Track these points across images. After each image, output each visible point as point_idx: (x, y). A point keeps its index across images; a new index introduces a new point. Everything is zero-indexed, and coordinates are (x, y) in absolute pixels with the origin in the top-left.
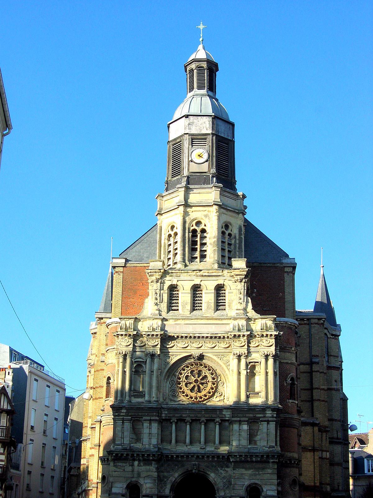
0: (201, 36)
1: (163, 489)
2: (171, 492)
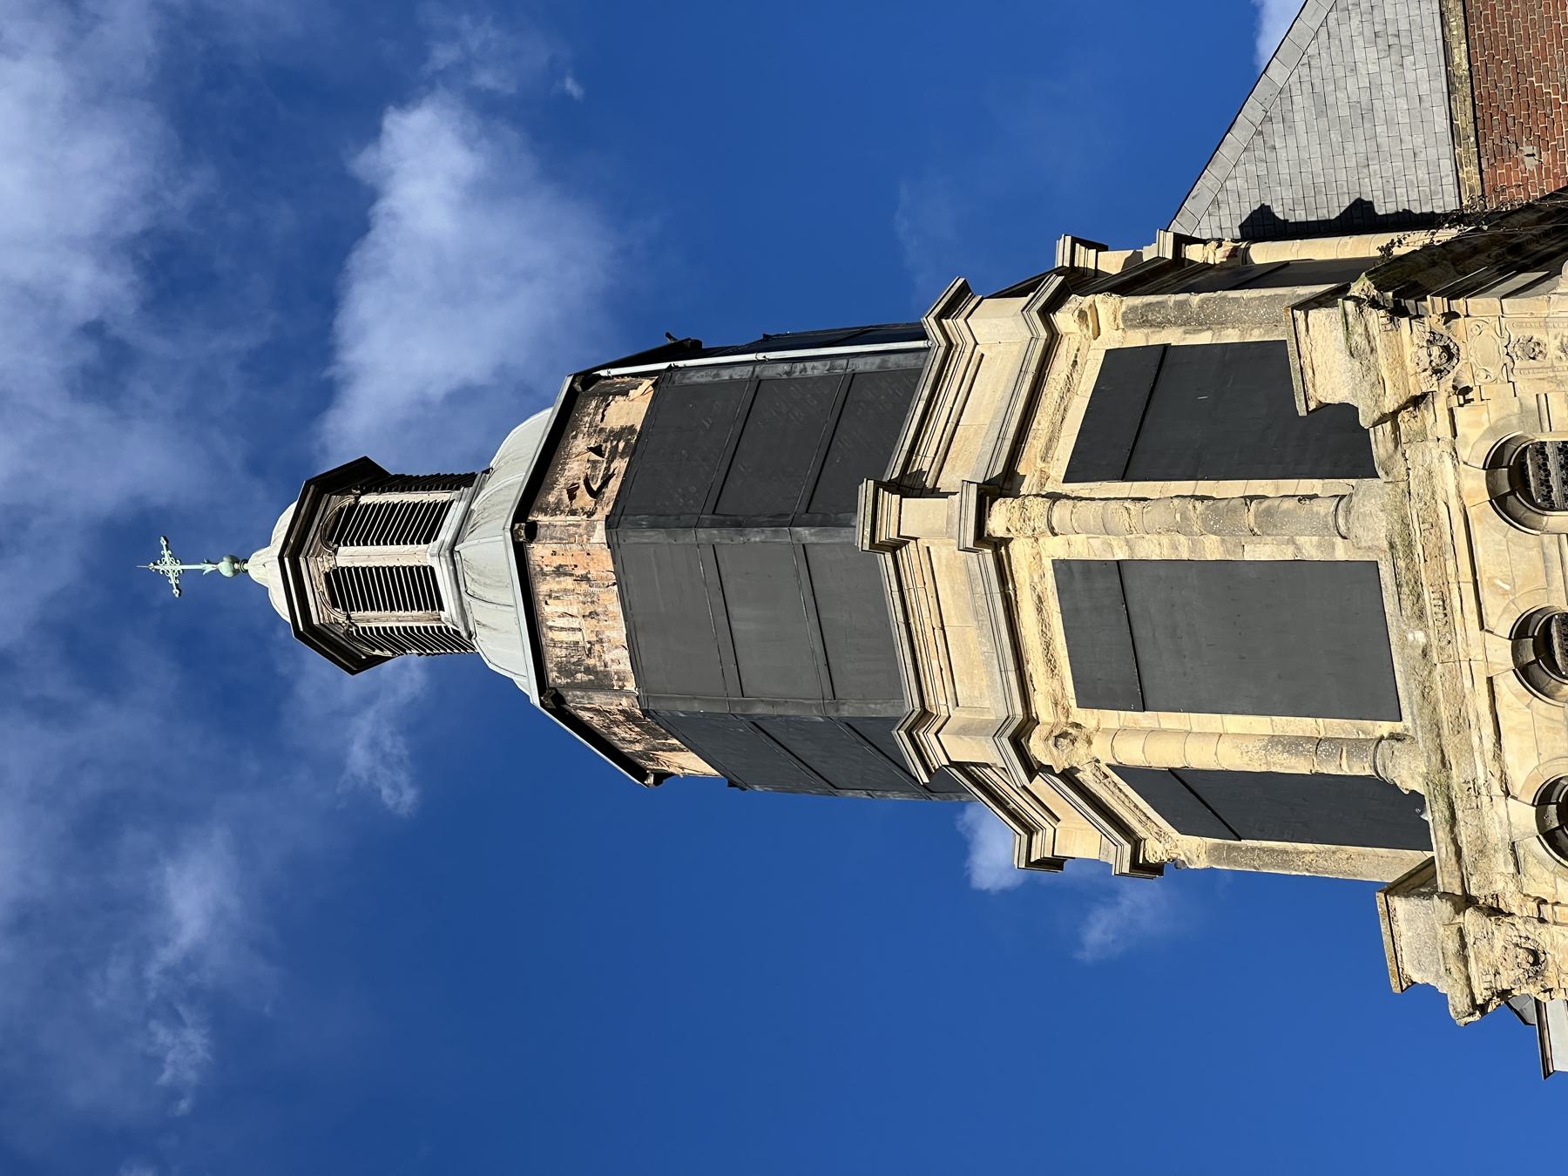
0: (209, 568)
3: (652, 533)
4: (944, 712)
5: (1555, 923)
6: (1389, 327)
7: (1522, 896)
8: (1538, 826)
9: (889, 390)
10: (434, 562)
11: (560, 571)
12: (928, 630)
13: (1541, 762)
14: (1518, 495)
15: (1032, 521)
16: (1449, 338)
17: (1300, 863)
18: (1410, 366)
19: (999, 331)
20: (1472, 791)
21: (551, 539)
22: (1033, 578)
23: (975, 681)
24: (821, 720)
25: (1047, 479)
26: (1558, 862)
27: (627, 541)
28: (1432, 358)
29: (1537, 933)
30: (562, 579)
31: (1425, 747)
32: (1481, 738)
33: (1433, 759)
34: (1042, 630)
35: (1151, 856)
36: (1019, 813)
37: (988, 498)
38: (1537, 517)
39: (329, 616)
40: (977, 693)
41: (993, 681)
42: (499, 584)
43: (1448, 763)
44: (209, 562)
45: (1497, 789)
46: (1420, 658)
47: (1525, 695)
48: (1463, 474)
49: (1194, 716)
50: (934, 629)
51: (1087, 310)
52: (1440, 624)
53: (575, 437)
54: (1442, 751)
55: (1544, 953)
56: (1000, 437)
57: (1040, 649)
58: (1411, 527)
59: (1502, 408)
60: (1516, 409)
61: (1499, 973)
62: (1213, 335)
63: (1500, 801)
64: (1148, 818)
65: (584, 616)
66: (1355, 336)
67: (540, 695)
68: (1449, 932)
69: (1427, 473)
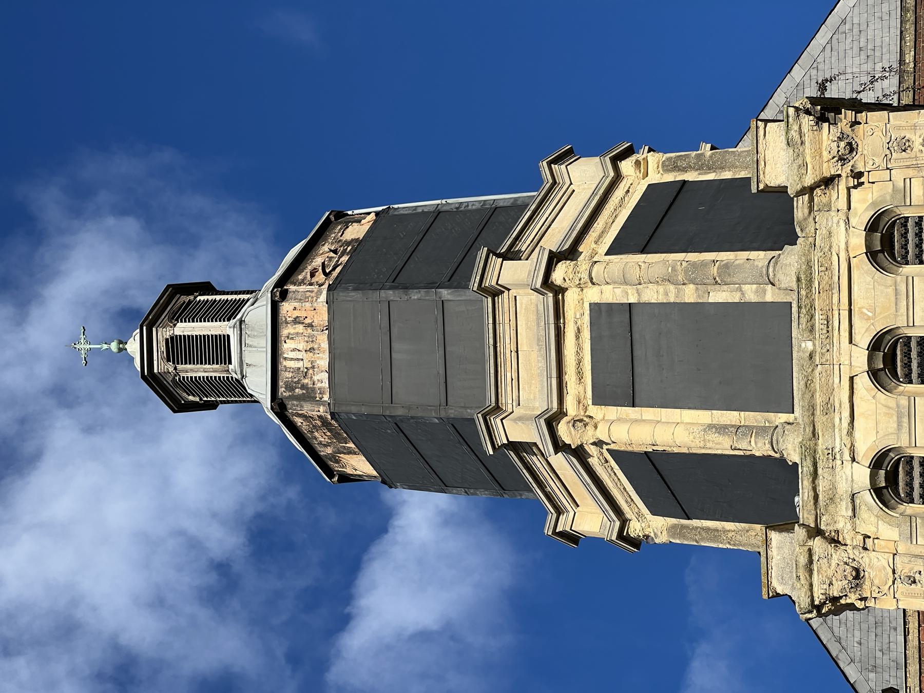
3: (353, 294)
4: (510, 409)
5: (874, 551)
6: (815, 128)
7: (855, 532)
8: (870, 482)
9: (515, 216)
10: (230, 332)
11: (296, 321)
12: (508, 352)
13: (878, 438)
14: (886, 254)
15: (580, 274)
16: (852, 138)
17: (725, 538)
18: (826, 156)
19: (586, 174)
20: (831, 457)
21: (295, 300)
22: (576, 315)
23: (532, 388)
24: (437, 421)
25: (596, 254)
26: (881, 509)
27: (339, 300)
28: (839, 149)
29: (860, 557)
30: (297, 326)
31: (803, 421)
32: (841, 419)
33: (807, 430)
34: (577, 351)
35: (632, 531)
36: (552, 496)
37: (555, 259)
38: (896, 268)
39: (164, 368)
40: (532, 397)
41: (542, 387)
42: (261, 334)
43: (817, 434)
44: (106, 343)
45: (847, 457)
46: (807, 359)
47: (872, 389)
48: (851, 234)
49: (664, 411)
50: (511, 351)
51: (641, 161)
52: (823, 337)
53: (324, 245)
54: (814, 426)
55: (864, 571)
56: (572, 228)
57: (574, 364)
58: (813, 268)
59: (881, 189)
60: (890, 190)
61: (832, 585)
62: (716, 175)
63: (848, 464)
64: (632, 500)
65: (306, 351)
66: (792, 132)
67: (271, 402)
68: (802, 550)
69: (828, 233)
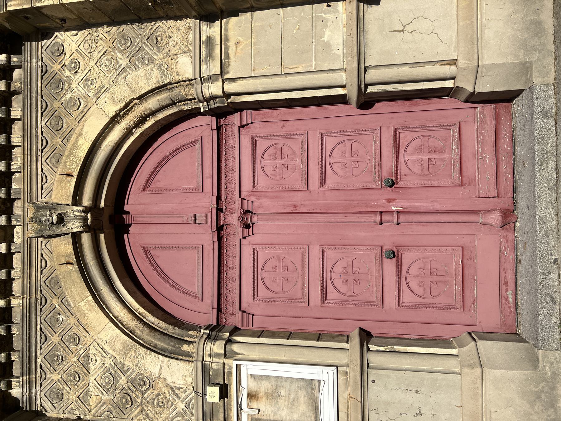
1: (168, 394)
2: (186, 347)
